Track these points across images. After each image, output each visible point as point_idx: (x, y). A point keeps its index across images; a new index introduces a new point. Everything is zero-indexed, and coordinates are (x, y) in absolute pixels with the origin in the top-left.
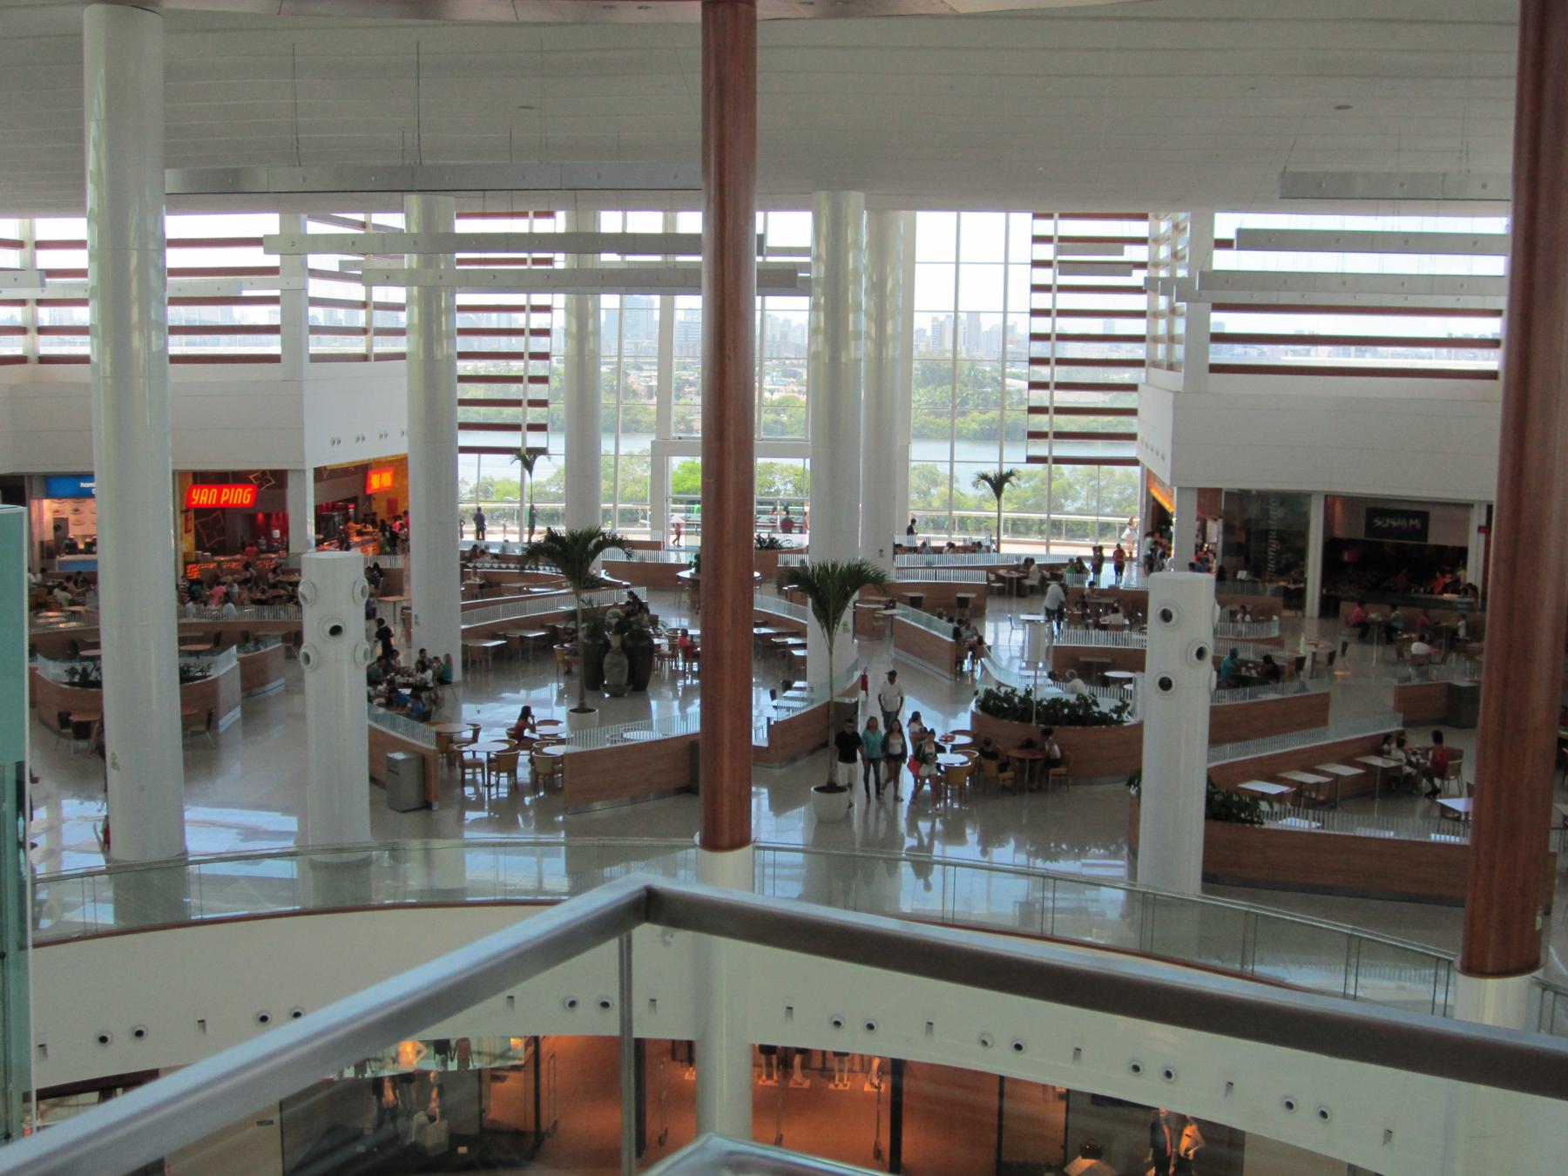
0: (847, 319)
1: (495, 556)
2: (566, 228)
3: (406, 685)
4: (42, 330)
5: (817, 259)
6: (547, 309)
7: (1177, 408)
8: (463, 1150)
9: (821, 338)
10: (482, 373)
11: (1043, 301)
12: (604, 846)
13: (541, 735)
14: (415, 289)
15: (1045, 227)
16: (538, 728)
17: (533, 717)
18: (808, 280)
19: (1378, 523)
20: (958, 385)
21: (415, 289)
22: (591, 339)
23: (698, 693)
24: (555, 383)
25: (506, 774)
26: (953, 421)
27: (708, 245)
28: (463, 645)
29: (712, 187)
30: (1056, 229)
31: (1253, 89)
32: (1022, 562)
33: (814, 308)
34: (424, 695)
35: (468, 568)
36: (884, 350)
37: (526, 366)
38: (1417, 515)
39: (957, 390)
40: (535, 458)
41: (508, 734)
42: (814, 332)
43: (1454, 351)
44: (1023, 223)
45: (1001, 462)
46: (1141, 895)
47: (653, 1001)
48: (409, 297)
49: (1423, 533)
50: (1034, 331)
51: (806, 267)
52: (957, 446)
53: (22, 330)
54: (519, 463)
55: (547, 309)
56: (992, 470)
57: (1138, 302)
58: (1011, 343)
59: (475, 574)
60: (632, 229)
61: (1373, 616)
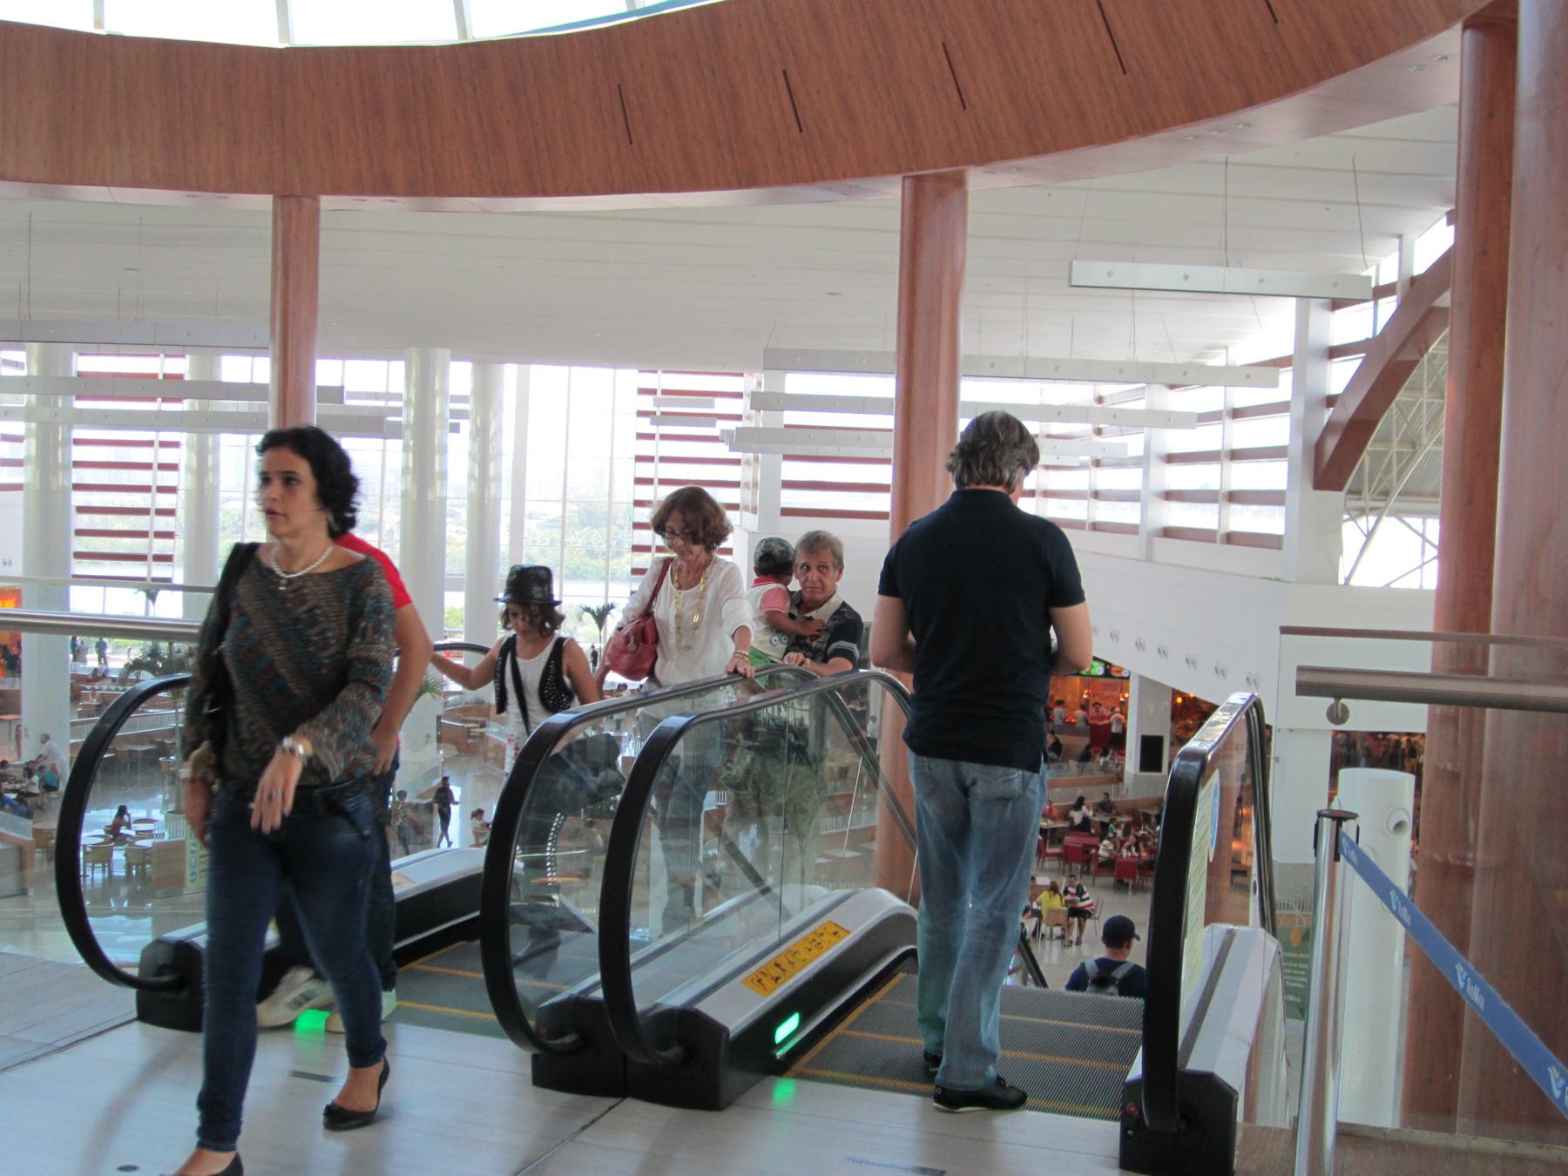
0: (434, 459)
1: (114, 680)
3: (13, 791)
5: (408, 403)
6: (176, 445)
9: (409, 478)
10: (129, 505)
11: (647, 448)
12: (177, 915)
13: (137, 832)
14: (33, 425)
15: (650, 381)
16: (133, 825)
17: (129, 815)
18: (398, 425)
20: (614, 528)
21: (33, 425)
23: (601, 986)
24: (181, 513)
25: (100, 865)
26: (608, 564)
27: (273, 393)
29: (277, 348)
31: (754, 276)
32: (616, 688)
33: (406, 449)
34: (30, 801)
35: (86, 689)
36: (487, 492)
37: (153, 500)
39: (612, 533)
40: (158, 591)
41: (106, 831)
44: (632, 378)
45: (606, 596)
48: (28, 430)
50: (638, 476)
51: (398, 412)
52: (611, 586)
54: (143, 595)
55: (176, 445)
56: (597, 604)
57: (721, 451)
59: (93, 695)
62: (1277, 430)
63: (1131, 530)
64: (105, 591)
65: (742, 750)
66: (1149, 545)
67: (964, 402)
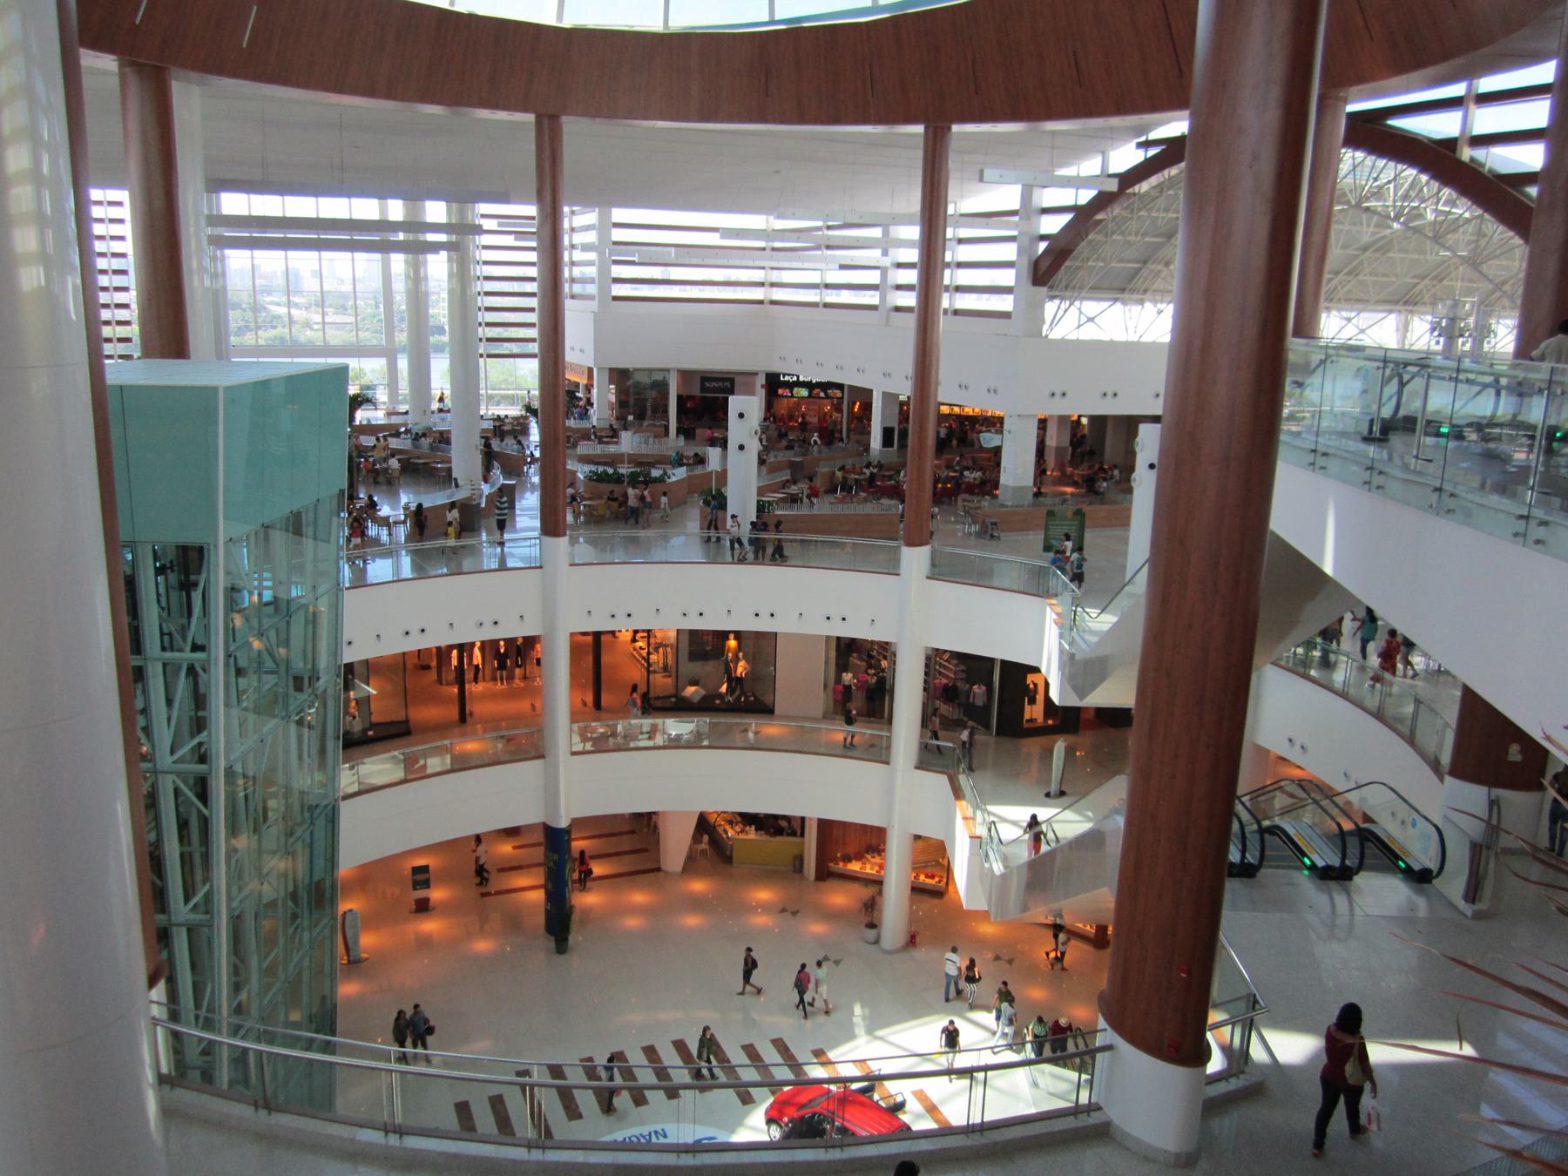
2: (405, 216)
7: (595, 320)
8: (371, 733)
9: (455, 280)
19: (707, 385)
22: (423, 284)
28: (758, 502)
30: (107, 228)
42: (450, 275)
43: (652, 286)
46: (510, 565)
47: (378, 636)
53: (762, 284)
58: (261, 277)
61: (716, 435)
62: (1009, 252)
63: (873, 308)
64: (284, 212)
65: (1497, 858)
66: (888, 317)
67: (914, 224)
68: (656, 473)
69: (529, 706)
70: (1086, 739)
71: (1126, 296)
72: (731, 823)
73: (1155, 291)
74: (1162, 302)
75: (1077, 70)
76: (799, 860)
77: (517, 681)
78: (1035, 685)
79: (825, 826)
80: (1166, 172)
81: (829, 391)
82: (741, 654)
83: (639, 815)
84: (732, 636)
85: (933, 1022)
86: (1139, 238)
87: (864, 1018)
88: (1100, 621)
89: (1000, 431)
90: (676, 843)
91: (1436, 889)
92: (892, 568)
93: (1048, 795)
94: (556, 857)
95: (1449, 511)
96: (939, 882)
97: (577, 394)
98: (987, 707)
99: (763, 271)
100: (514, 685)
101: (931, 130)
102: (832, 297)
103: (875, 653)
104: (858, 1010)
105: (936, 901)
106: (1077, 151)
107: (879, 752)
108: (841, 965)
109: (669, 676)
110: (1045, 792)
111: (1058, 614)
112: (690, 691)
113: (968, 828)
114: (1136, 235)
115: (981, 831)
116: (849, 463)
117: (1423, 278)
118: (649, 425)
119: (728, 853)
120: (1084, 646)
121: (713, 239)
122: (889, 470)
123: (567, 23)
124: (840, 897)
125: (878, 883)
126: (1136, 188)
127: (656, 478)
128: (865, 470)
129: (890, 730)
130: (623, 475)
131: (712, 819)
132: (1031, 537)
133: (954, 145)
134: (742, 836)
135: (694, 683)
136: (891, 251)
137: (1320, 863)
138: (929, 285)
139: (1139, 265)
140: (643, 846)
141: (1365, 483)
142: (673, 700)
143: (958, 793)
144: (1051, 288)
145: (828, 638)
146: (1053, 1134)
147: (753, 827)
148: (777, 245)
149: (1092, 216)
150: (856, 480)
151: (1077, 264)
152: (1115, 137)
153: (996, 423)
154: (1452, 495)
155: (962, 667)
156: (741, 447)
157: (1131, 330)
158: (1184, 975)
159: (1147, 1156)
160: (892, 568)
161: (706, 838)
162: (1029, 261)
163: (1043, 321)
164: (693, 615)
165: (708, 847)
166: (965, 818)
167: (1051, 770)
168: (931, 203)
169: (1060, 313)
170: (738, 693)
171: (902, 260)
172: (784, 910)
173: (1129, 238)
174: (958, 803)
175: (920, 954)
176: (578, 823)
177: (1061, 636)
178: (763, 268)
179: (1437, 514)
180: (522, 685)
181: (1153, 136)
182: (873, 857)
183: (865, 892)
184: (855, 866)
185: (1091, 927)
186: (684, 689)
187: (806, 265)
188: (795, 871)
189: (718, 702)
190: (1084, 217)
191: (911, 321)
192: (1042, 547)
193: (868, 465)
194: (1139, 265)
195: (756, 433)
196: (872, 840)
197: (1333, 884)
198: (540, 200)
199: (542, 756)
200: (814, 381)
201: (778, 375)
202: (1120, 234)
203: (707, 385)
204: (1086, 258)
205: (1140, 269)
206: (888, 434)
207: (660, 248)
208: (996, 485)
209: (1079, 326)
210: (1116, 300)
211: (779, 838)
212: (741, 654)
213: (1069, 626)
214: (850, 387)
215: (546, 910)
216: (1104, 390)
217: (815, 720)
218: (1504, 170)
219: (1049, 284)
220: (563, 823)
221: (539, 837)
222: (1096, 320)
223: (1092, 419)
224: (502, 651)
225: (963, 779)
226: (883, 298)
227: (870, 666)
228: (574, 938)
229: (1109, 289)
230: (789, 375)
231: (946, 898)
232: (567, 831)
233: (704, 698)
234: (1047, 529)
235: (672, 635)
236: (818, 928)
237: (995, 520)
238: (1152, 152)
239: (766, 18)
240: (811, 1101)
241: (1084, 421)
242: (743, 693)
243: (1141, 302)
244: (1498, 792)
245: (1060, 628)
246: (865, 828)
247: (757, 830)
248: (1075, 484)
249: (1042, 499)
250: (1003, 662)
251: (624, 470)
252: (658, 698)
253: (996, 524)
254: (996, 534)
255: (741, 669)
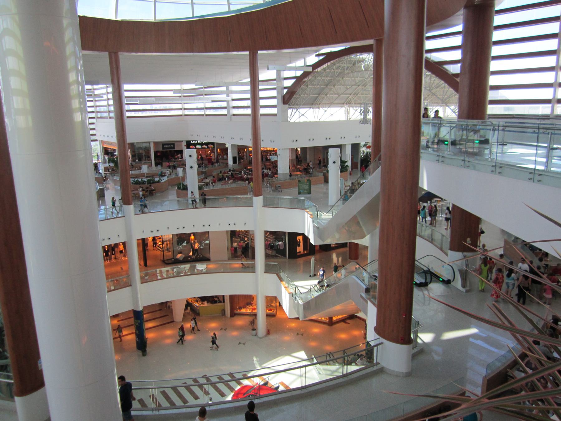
4: (185, 109)
19: (165, 146)
38: (172, 145)
49: (174, 148)
53: (181, 109)
60: (179, 85)
61: (170, 164)
62: (274, 93)
66: (231, 118)
68: (157, 179)
69: (120, 268)
70: (318, 256)
71: (313, 106)
72: (197, 301)
73: (323, 104)
74: (326, 107)
75: (301, 32)
76: (223, 311)
77: (113, 260)
78: (299, 240)
79: (232, 297)
80: (326, 64)
81: (209, 146)
82: (196, 241)
83: (162, 303)
84: (192, 235)
85: (281, 358)
86: (319, 87)
87: (258, 361)
88: (326, 216)
89: (276, 155)
90: (179, 312)
91: (453, 285)
92: (251, 205)
93: (310, 276)
94: (139, 321)
95: (468, 166)
96: (274, 311)
97: (115, 153)
98: (285, 249)
99: (181, 104)
100: (112, 262)
101: (251, 53)
102: (209, 112)
103: (241, 236)
104: (255, 359)
105: (273, 318)
106: (297, 58)
107: (252, 269)
108: (246, 345)
109: (169, 252)
110: (309, 275)
111: (310, 215)
112: (179, 256)
113: (287, 291)
114: (318, 85)
115: (292, 291)
116: (223, 171)
117: (351, 94)
118: (144, 163)
119: (198, 312)
120: (323, 224)
121: (171, 94)
122: (237, 171)
123: (119, 19)
124: (240, 322)
125: (255, 315)
126: (317, 70)
127: (157, 181)
128: (229, 172)
129: (255, 261)
130: (145, 181)
131: (190, 301)
132: (292, 190)
133: (259, 58)
134: (202, 305)
135: (180, 253)
136: (230, 95)
137: (418, 282)
138: (255, 106)
139: (317, 96)
140: (166, 314)
141: (437, 160)
142: (173, 260)
143: (281, 280)
144: (289, 105)
145: (227, 231)
146: (367, 373)
147: (206, 302)
148: (185, 95)
149: (302, 80)
150: (227, 176)
151: (298, 96)
152: (309, 53)
153: (275, 152)
154: (469, 162)
155: (274, 237)
156: (191, 167)
157: (316, 118)
158: (404, 316)
159: (397, 375)
160: (251, 205)
161: (189, 308)
162: (281, 96)
163: (288, 116)
164: (181, 228)
165: (190, 311)
166: (286, 287)
167: (311, 267)
168: (254, 78)
169: (293, 113)
170: (196, 254)
171: (234, 98)
172: (221, 329)
173: (315, 87)
174: (282, 283)
175: (271, 337)
176: (145, 308)
177: (313, 222)
178: (181, 103)
179: (464, 168)
180: (115, 261)
181: (321, 52)
182: (249, 306)
183: (249, 319)
184: (244, 311)
185: (327, 319)
186: (177, 255)
187: (195, 102)
188: (222, 315)
189: (189, 259)
190: (299, 80)
191: (250, 119)
192: (297, 193)
193: (230, 171)
194: (317, 96)
195: (196, 162)
196: (249, 300)
197: (422, 288)
198: (113, 82)
199: (131, 285)
200: (204, 142)
201: (191, 141)
202: (312, 85)
203: (165, 146)
204: (301, 94)
205: (318, 97)
206: (234, 159)
207: (145, 98)
208: (276, 173)
209: (299, 117)
210: (310, 108)
211: (215, 304)
212: (196, 241)
213: (315, 219)
214: (217, 143)
215: (136, 341)
216: (309, 138)
217: (225, 261)
218: (437, 60)
219: (289, 103)
220: (140, 309)
221: (132, 315)
222: (304, 115)
223: (302, 149)
224: (107, 249)
225: (282, 274)
226: (228, 112)
227: (241, 240)
228: (148, 350)
229: (308, 104)
230: (194, 141)
231: (276, 317)
232: (142, 311)
233: (184, 258)
234: (298, 187)
235: (171, 237)
236: (235, 333)
237: (279, 185)
238: (321, 58)
239: (191, 16)
240: (247, 391)
241: (299, 149)
242: (198, 254)
243: (319, 108)
244: (465, 253)
245: (313, 219)
246: (245, 296)
247: (207, 302)
248: (300, 171)
249: (293, 177)
250: (289, 233)
251: (145, 179)
252: (167, 260)
253: (280, 187)
254: (280, 190)
255: (197, 246)
